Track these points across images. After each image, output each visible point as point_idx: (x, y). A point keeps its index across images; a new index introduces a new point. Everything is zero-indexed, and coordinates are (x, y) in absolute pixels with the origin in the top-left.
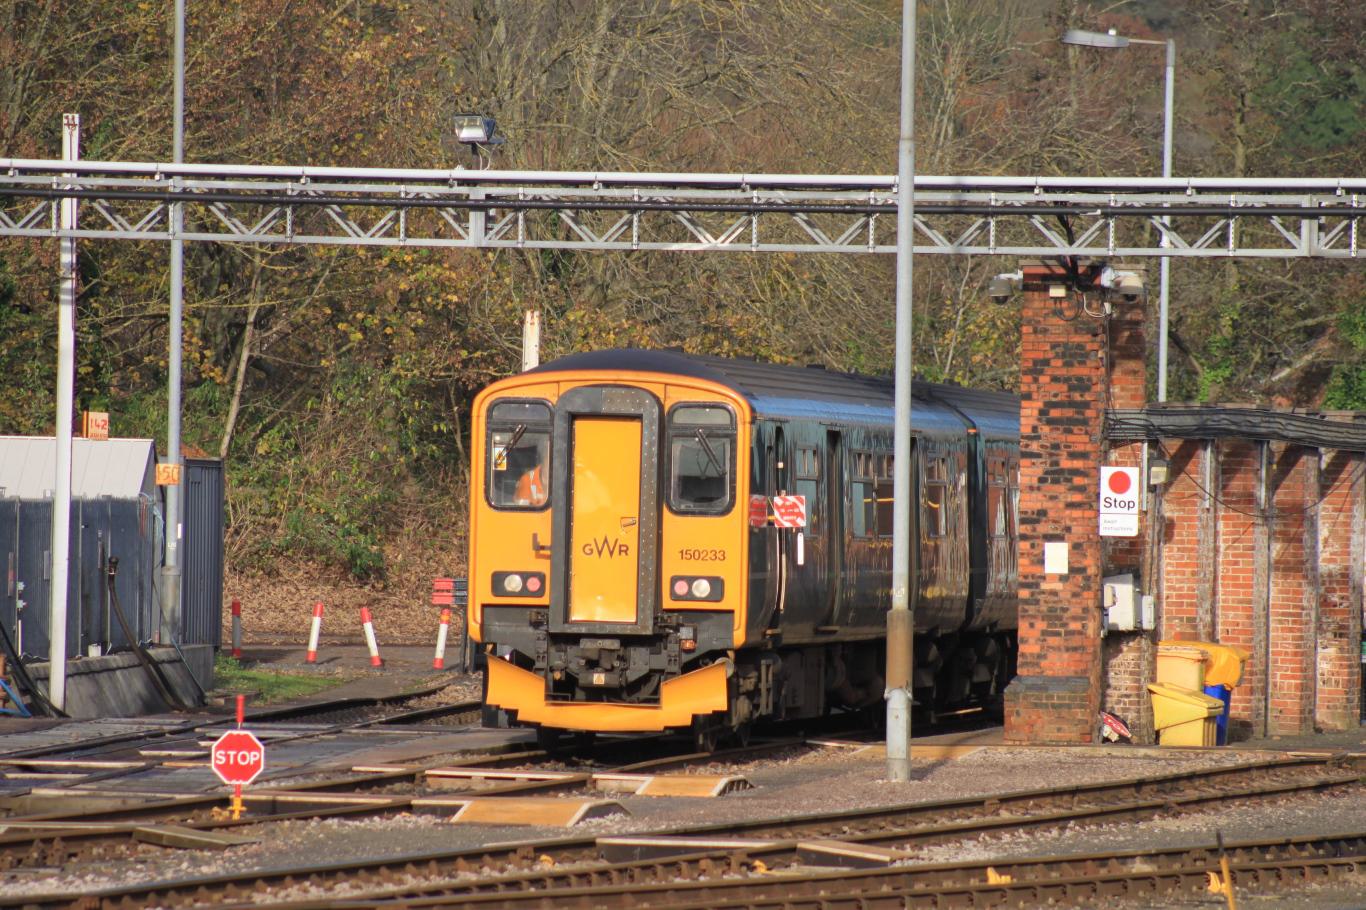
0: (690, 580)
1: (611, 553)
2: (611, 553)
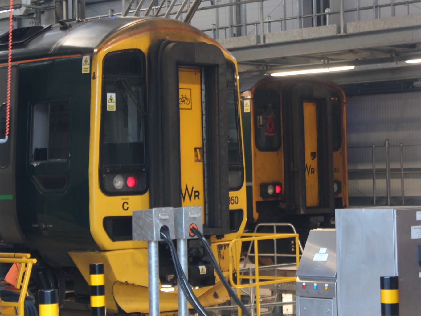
1: (190, 197)
2: (190, 197)
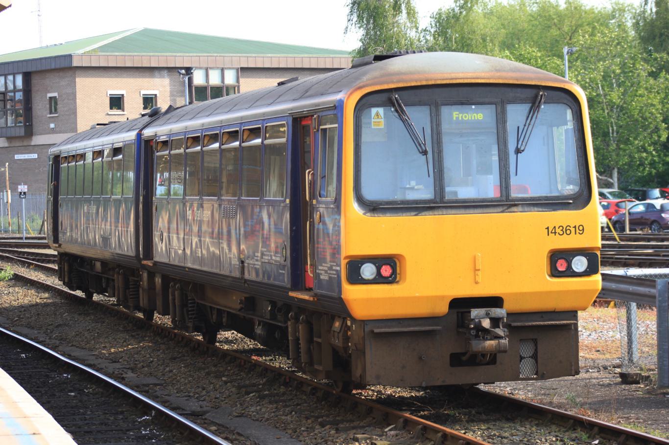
0: (380, 279)
